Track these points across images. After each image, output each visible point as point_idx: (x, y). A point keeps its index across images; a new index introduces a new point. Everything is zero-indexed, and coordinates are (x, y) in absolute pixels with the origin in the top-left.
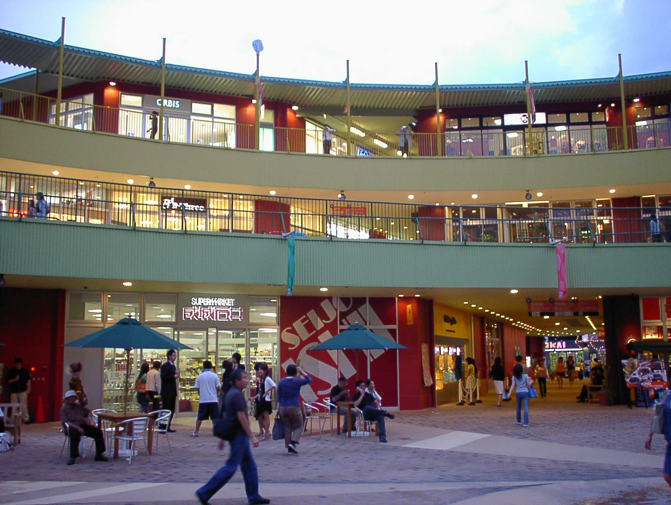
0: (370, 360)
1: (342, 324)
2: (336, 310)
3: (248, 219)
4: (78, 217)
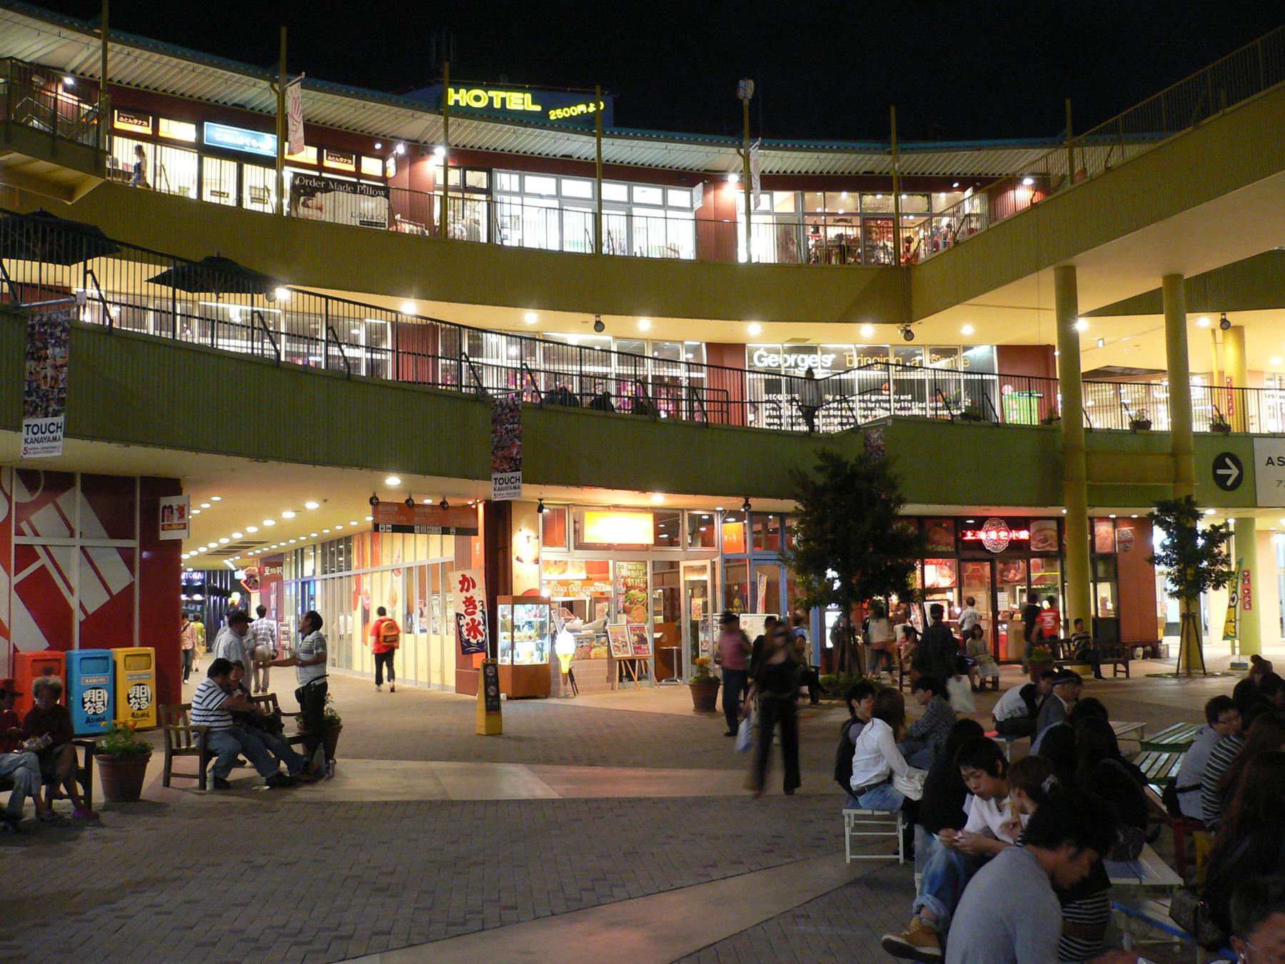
0: (78, 616)
1: (20, 533)
2: (9, 499)
3: (578, 358)
4: (163, 333)
